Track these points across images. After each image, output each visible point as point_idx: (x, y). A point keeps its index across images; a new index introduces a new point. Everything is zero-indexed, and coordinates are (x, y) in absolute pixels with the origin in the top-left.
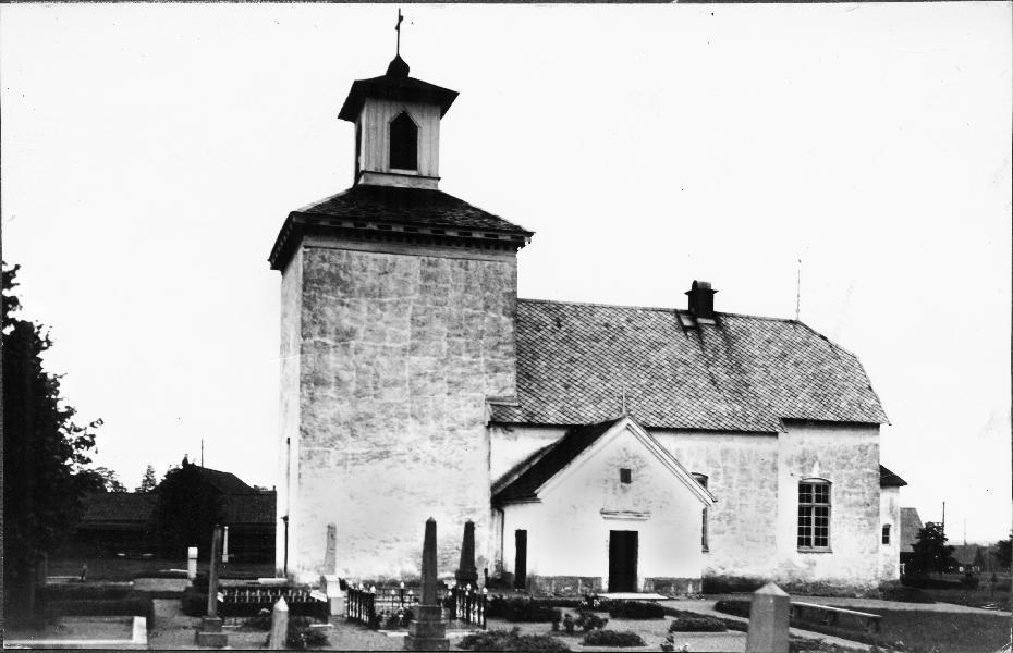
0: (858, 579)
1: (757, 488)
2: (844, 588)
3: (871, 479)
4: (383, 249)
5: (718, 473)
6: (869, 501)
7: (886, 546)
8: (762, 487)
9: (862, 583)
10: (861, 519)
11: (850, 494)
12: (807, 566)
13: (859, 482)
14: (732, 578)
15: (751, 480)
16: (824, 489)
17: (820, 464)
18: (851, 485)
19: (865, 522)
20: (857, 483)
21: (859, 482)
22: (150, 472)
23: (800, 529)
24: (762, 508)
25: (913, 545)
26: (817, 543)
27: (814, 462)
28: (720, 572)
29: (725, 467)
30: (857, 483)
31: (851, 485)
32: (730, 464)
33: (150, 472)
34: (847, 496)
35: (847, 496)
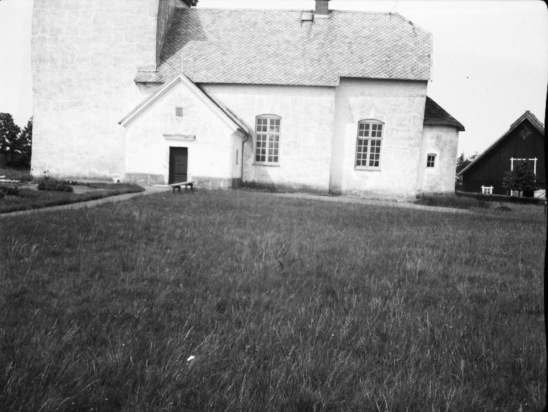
2: (389, 195)
6: (412, 136)
7: (430, 169)
9: (403, 192)
11: (398, 131)
14: (295, 184)
16: (378, 129)
17: (376, 109)
18: (400, 125)
20: (403, 123)
31: (400, 125)
34: (395, 132)
35: (395, 132)
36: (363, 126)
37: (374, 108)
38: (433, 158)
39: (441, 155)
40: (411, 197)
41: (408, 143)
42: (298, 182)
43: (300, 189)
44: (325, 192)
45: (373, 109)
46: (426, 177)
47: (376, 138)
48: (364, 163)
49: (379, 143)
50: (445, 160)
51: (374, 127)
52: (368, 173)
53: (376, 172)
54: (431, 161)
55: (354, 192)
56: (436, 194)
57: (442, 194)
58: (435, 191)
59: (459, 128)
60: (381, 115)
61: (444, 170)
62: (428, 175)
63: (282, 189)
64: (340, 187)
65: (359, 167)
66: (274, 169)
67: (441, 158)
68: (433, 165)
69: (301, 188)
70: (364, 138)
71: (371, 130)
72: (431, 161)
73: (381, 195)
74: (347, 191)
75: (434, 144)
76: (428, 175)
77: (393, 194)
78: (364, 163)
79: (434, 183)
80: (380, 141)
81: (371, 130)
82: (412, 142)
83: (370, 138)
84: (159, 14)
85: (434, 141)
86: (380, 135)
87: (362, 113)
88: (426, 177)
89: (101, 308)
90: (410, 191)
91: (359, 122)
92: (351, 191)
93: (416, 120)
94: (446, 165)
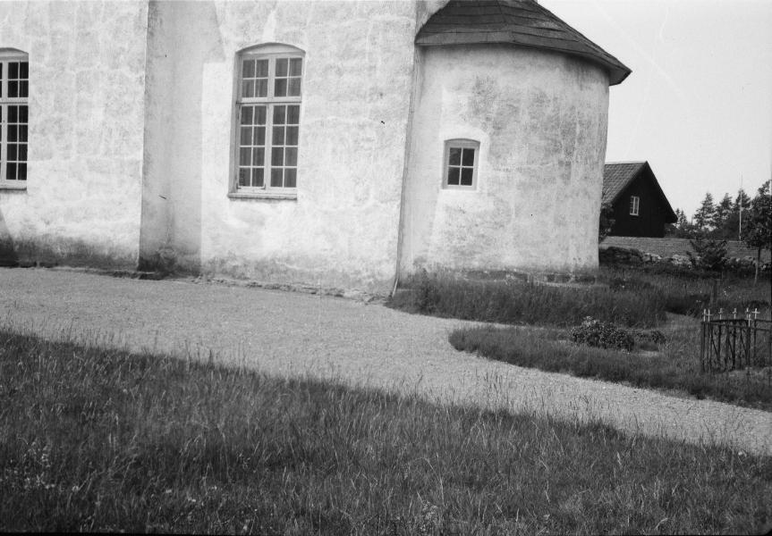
0: (351, 258)
1: (106, 68)
2: (321, 276)
3: (391, 35)
4: (459, 142)
5: (43, 45)
6: (382, 85)
7: (458, 193)
8: (115, 66)
9: (359, 267)
10: (362, 127)
11: (340, 72)
12: (246, 226)
13: (363, 43)
14: (61, 241)
15: (97, 52)
16: (290, 71)
17: (280, 15)
18: (346, 54)
19: (371, 133)
20: (357, 46)
21: (363, 43)
22: (709, 198)
23: (25, 138)
24: (115, 107)
25: (343, 270)
26: (276, 182)
27: (268, 12)
28: (41, 229)
29: (54, 34)
30: (357, 46)
31: (346, 54)
32: (64, 27)
33: (709, 198)
34: (332, 77)
35: (332, 77)
36: (249, 66)
37: (273, 14)
38: (469, 156)
39: (493, 145)
40: (380, 284)
41: (370, 106)
42: (66, 235)
43: (70, 255)
44: (121, 263)
45: (272, 16)
46: (440, 216)
47: (288, 99)
48: (259, 180)
49: (294, 113)
50: (515, 159)
51: (281, 64)
52: (264, 208)
53: (283, 203)
54: (461, 167)
55: (230, 265)
56: (472, 273)
57: (500, 274)
58: (476, 264)
59: (614, 72)
60: (294, 29)
61: (512, 196)
62: (448, 209)
63: (30, 255)
64: (197, 251)
65: (245, 191)
66: (284, 206)
67: (495, 154)
68: (467, 179)
69: (73, 251)
70: (253, 101)
71: (272, 78)
72: (461, 167)
73: (302, 274)
74: (212, 262)
75: (465, 110)
76: (448, 209)
77: (333, 271)
78: (259, 180)
79: (470, 238)
80: (297, 108)
81: (272, 78)
82: (382, 104)
83: (271, 99)
84: (582, 35)
85: (464, 98)
86: (296, 90)
87: (244, 28)
88: (440, 216)
89: (33, 476)
90: (380, 263)
91: (240, 54)
92: (223, 262)
93: (391, 35)
94: (518, 177)
